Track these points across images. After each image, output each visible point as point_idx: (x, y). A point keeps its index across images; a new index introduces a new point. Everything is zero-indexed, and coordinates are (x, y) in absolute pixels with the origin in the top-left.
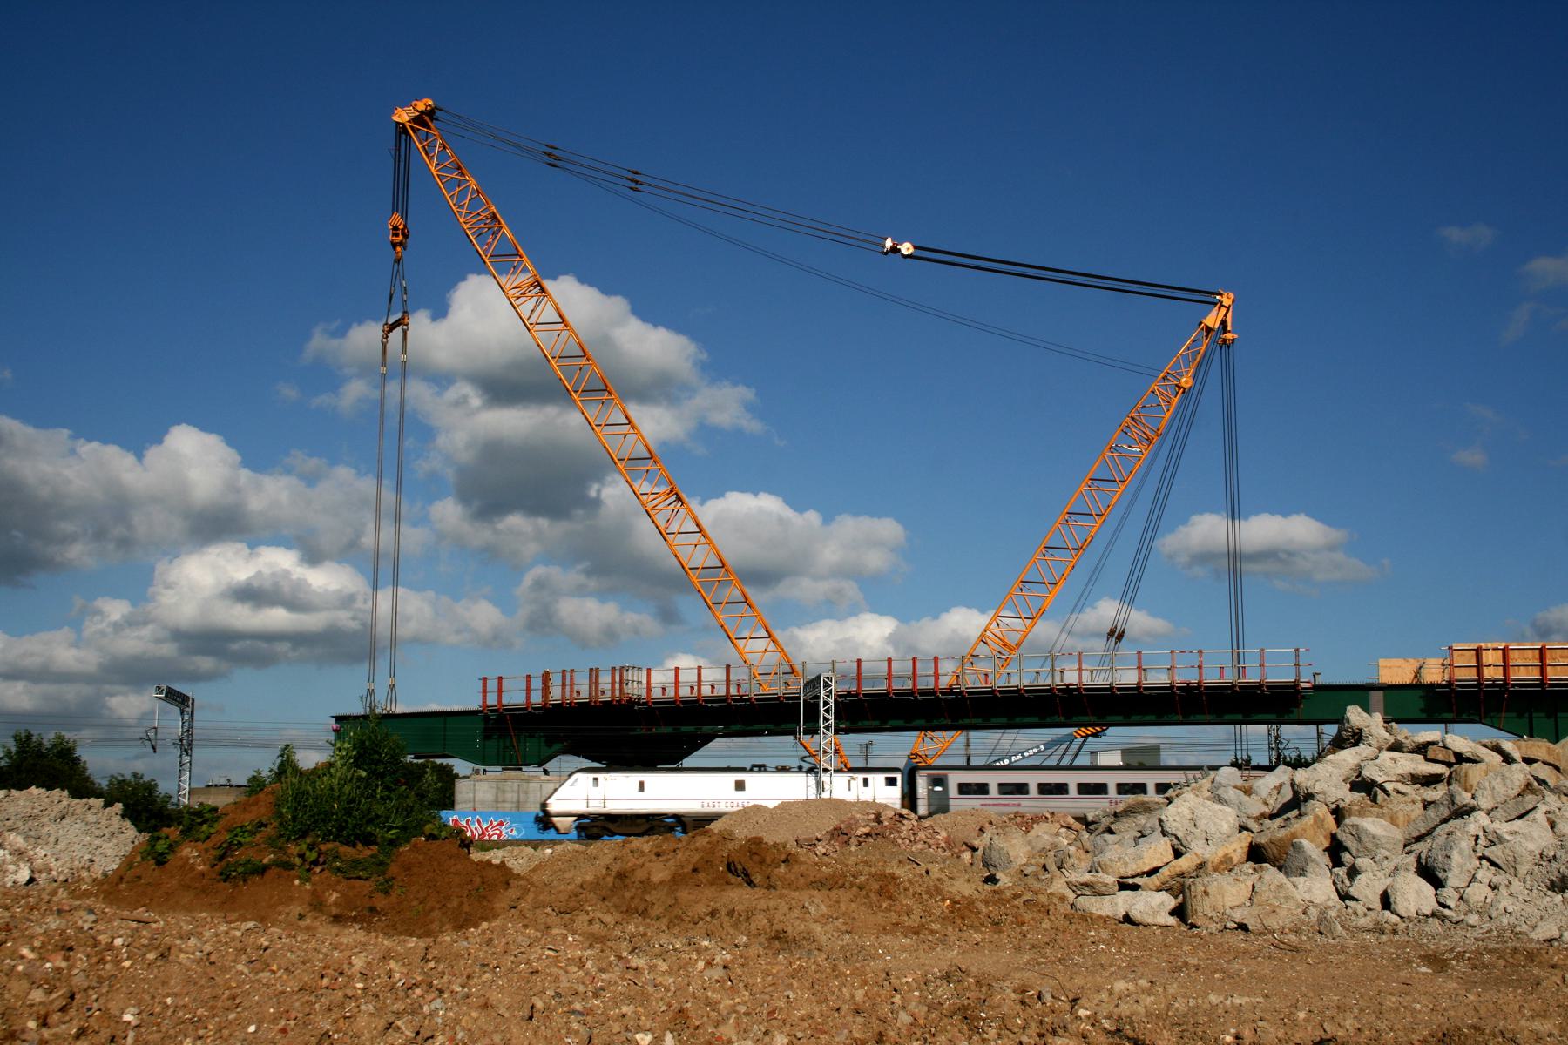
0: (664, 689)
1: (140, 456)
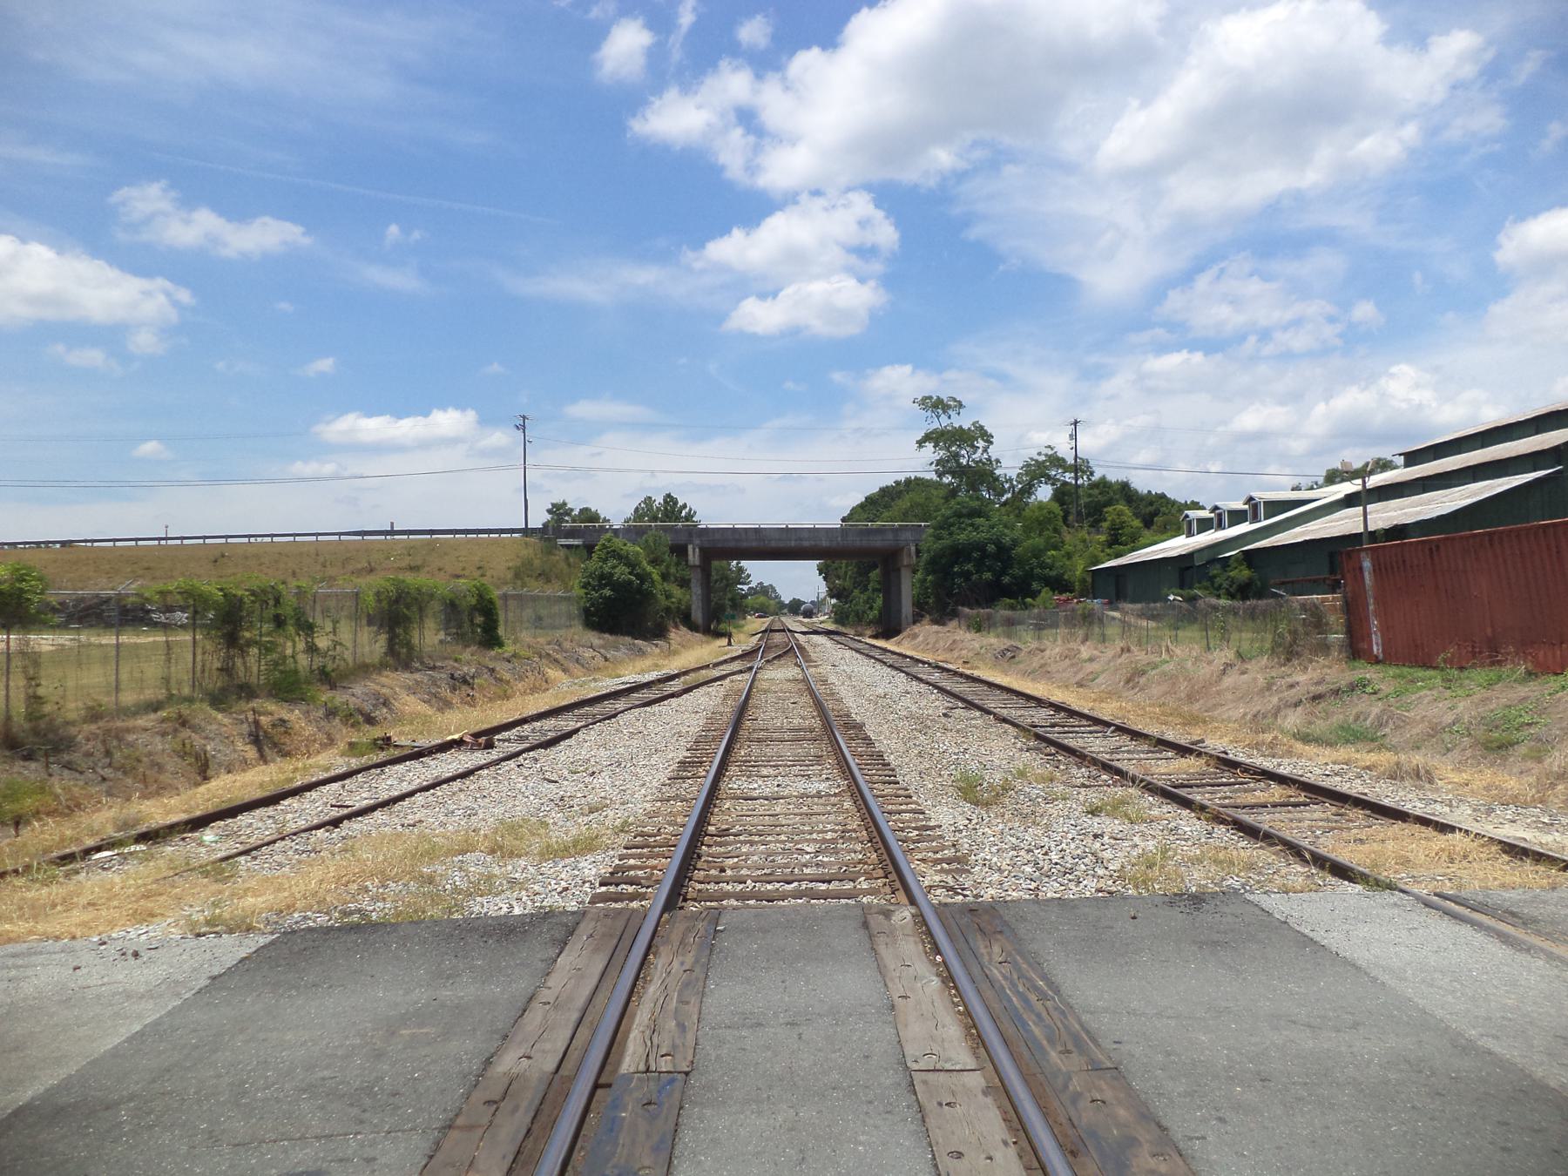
0: (392, 524)
1: (748, 234)
